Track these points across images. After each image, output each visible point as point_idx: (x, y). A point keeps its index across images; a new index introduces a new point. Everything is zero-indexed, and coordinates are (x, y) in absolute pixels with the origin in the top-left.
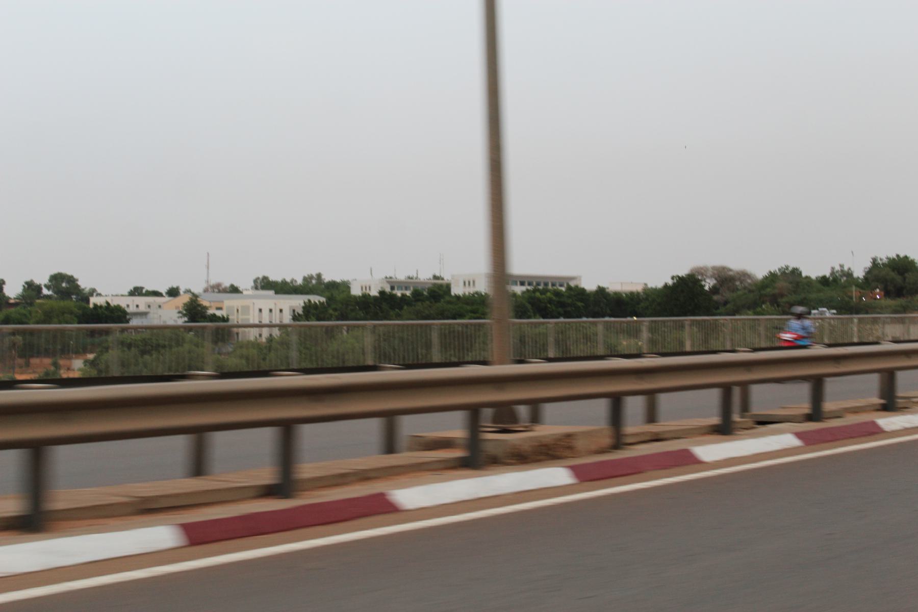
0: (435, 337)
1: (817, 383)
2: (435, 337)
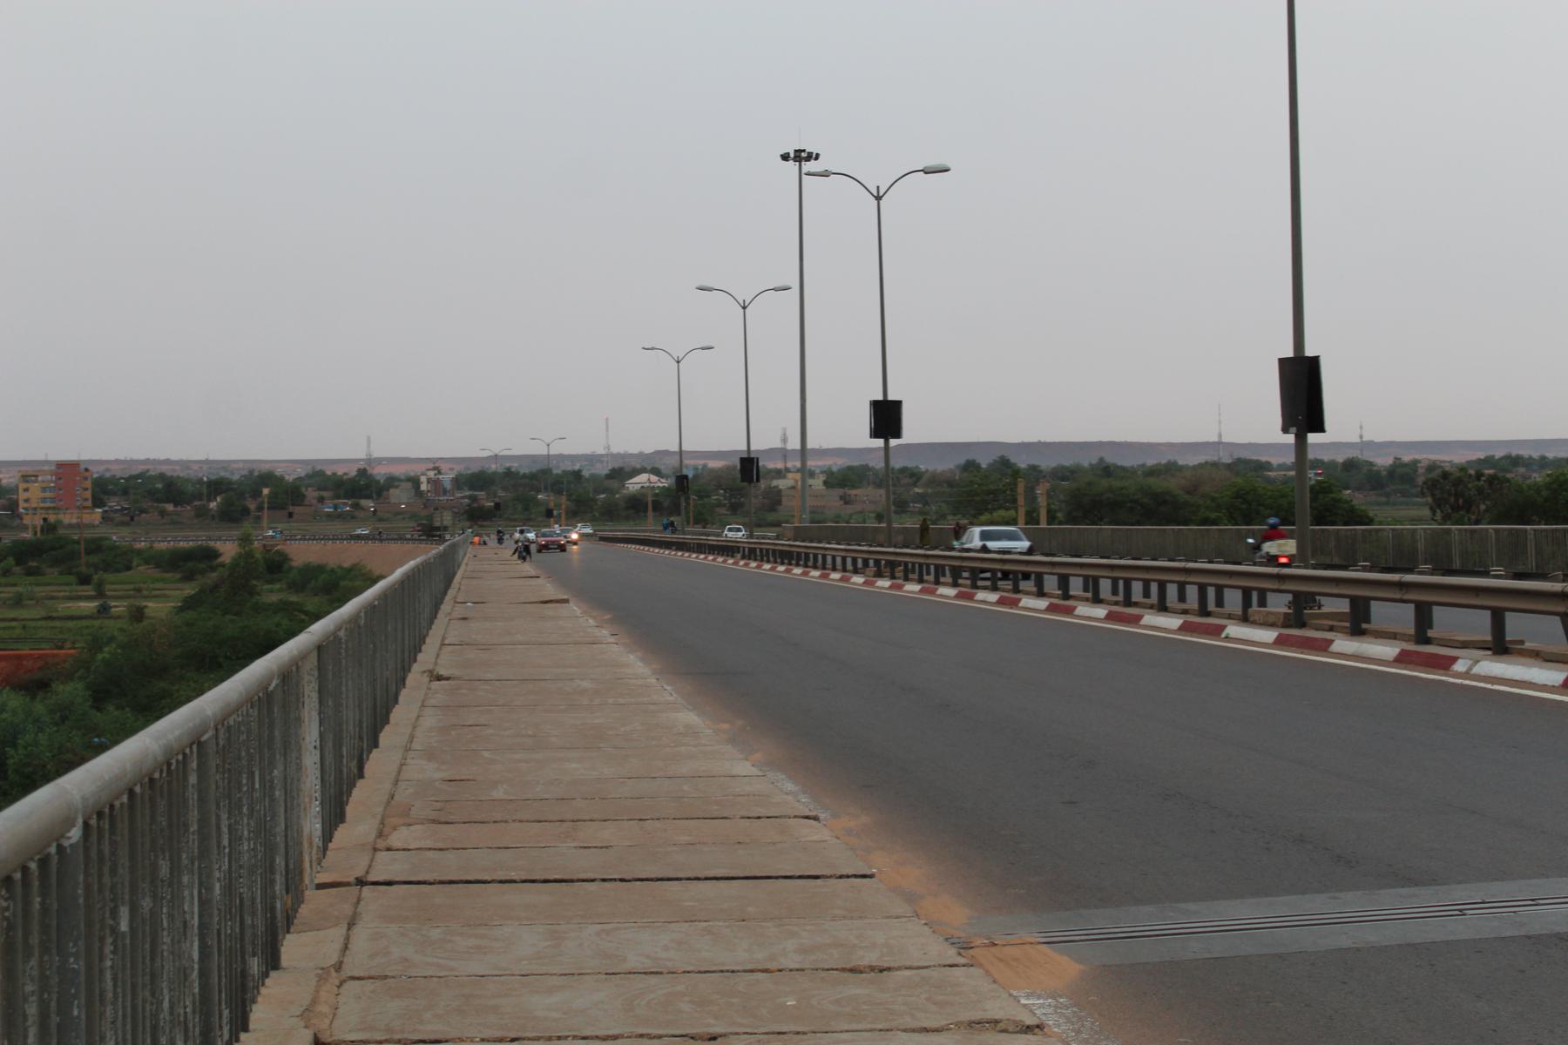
0: (1531, 537)
1: (1498, 618)
2: (1531, 537)
